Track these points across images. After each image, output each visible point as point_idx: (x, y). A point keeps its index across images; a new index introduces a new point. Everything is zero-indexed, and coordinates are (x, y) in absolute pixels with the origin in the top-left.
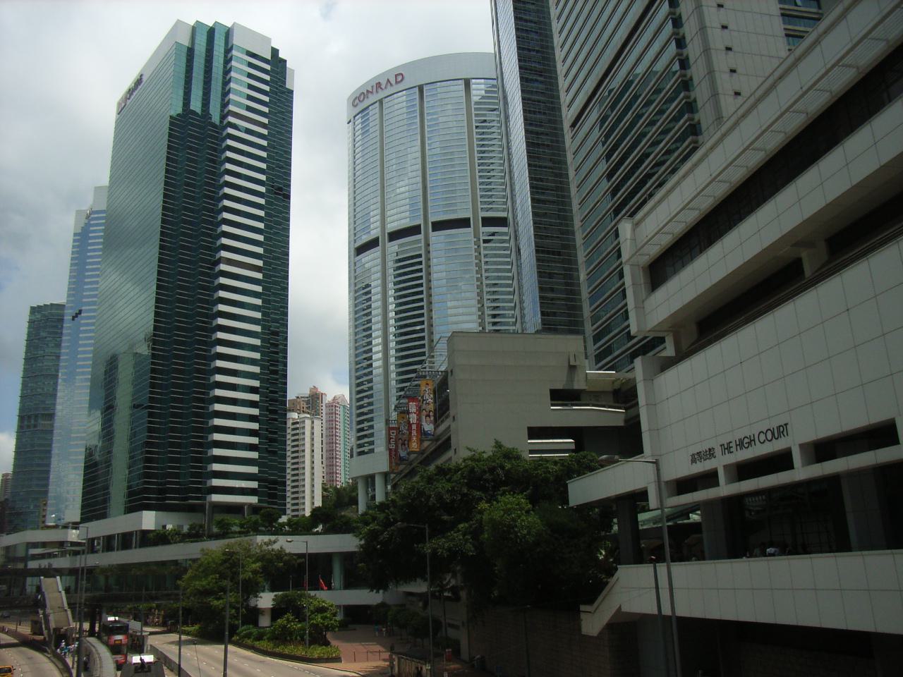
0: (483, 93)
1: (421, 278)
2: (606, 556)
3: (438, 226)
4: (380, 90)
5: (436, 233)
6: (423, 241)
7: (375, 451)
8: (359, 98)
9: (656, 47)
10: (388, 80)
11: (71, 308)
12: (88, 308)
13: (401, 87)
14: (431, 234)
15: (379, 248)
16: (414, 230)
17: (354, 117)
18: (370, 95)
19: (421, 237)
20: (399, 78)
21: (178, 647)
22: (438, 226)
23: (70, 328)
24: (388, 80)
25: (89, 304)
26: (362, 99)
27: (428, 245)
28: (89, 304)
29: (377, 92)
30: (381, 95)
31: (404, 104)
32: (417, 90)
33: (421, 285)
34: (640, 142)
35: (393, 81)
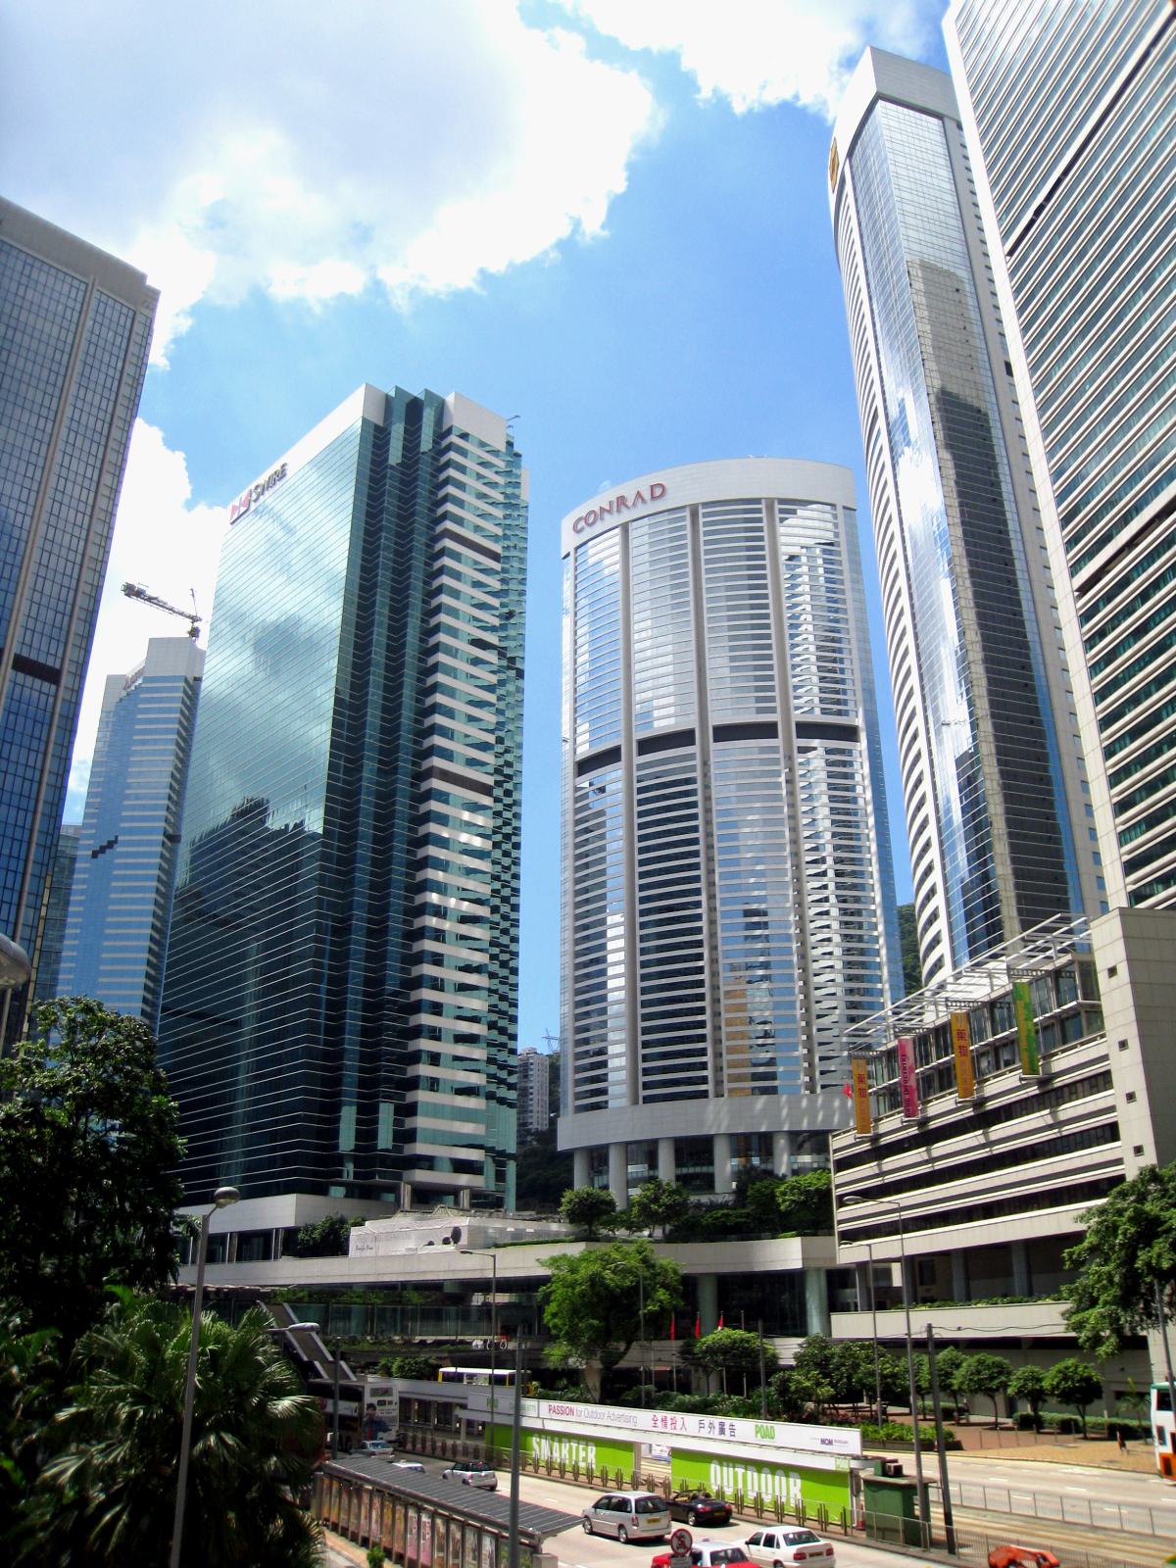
0: (647, 557)
1: (694, 817)
2: (37, 1266)
3: (724, 733)
4: (623, 509)
5: (721, 745)
6: (698, 756)
7: (610, 1105)
8: (586, 519)
9: (796, 531)
10: (639, 495)
11: (90, 837)
12: (127, 838)
13: (661, 505)
14: (713, 746)
15: (622, 764)
16: (684, 738)
17: (577, 548)
18: (606, 516)
19: (695, 749)
20: (658, 492)
21: (522, 1497)
22: (724, 733)
23: (85, 871)
24: (639, 495)
25: (130, 831)
26: (591, 520)
27: (705, 763)
28: (130, 831)
29: (619, 511)
30: (626, 516)
31: (646, 538)
32: (687, 513)
33: (695, 829)
34: (1134, 611)
35: (647, 496)
